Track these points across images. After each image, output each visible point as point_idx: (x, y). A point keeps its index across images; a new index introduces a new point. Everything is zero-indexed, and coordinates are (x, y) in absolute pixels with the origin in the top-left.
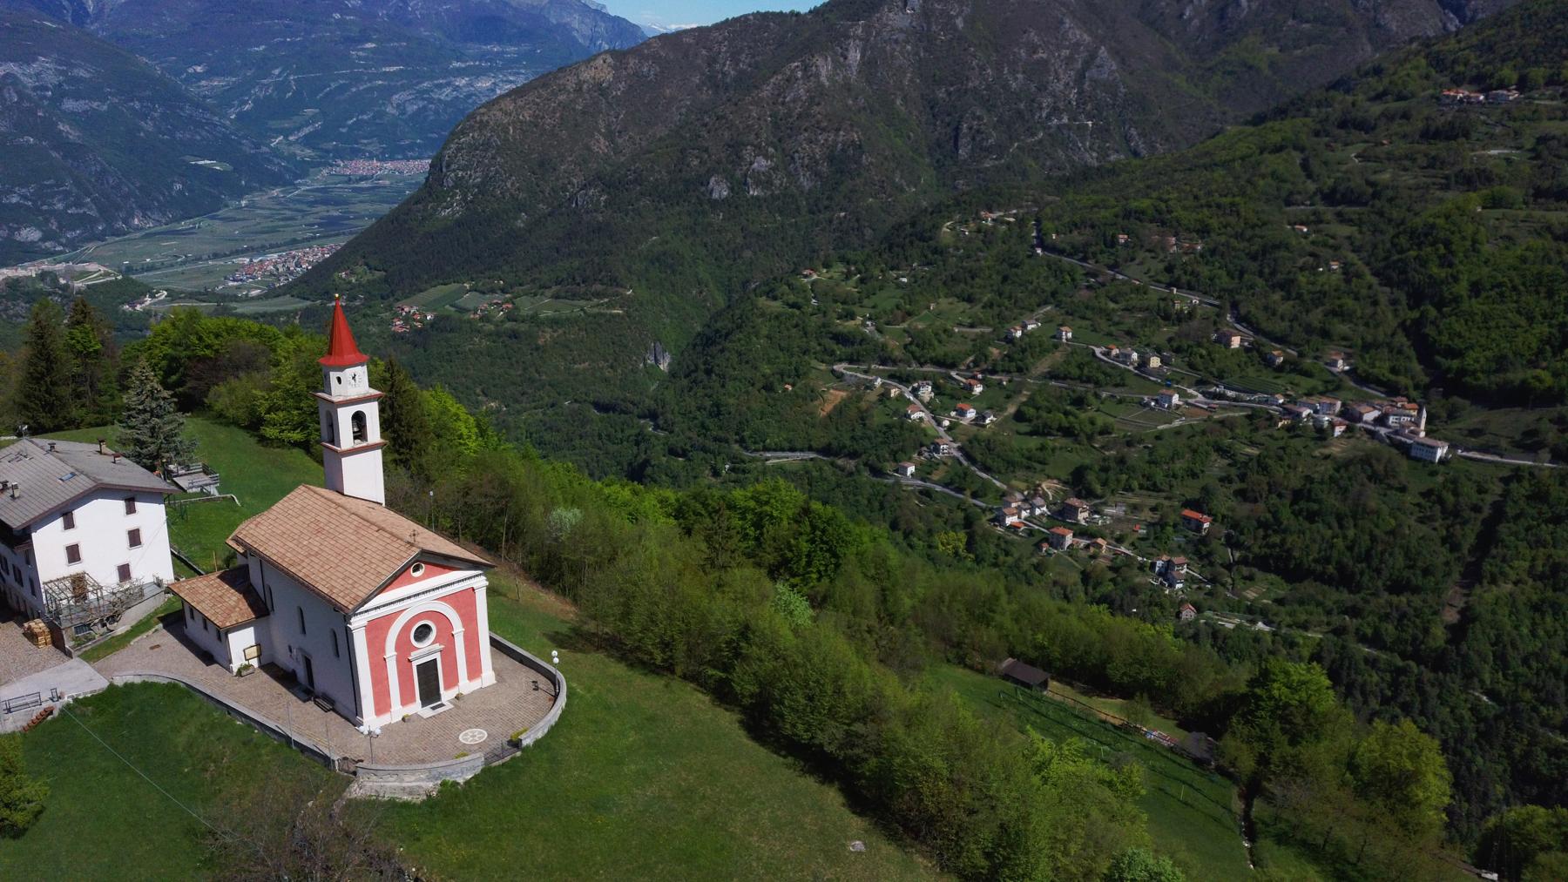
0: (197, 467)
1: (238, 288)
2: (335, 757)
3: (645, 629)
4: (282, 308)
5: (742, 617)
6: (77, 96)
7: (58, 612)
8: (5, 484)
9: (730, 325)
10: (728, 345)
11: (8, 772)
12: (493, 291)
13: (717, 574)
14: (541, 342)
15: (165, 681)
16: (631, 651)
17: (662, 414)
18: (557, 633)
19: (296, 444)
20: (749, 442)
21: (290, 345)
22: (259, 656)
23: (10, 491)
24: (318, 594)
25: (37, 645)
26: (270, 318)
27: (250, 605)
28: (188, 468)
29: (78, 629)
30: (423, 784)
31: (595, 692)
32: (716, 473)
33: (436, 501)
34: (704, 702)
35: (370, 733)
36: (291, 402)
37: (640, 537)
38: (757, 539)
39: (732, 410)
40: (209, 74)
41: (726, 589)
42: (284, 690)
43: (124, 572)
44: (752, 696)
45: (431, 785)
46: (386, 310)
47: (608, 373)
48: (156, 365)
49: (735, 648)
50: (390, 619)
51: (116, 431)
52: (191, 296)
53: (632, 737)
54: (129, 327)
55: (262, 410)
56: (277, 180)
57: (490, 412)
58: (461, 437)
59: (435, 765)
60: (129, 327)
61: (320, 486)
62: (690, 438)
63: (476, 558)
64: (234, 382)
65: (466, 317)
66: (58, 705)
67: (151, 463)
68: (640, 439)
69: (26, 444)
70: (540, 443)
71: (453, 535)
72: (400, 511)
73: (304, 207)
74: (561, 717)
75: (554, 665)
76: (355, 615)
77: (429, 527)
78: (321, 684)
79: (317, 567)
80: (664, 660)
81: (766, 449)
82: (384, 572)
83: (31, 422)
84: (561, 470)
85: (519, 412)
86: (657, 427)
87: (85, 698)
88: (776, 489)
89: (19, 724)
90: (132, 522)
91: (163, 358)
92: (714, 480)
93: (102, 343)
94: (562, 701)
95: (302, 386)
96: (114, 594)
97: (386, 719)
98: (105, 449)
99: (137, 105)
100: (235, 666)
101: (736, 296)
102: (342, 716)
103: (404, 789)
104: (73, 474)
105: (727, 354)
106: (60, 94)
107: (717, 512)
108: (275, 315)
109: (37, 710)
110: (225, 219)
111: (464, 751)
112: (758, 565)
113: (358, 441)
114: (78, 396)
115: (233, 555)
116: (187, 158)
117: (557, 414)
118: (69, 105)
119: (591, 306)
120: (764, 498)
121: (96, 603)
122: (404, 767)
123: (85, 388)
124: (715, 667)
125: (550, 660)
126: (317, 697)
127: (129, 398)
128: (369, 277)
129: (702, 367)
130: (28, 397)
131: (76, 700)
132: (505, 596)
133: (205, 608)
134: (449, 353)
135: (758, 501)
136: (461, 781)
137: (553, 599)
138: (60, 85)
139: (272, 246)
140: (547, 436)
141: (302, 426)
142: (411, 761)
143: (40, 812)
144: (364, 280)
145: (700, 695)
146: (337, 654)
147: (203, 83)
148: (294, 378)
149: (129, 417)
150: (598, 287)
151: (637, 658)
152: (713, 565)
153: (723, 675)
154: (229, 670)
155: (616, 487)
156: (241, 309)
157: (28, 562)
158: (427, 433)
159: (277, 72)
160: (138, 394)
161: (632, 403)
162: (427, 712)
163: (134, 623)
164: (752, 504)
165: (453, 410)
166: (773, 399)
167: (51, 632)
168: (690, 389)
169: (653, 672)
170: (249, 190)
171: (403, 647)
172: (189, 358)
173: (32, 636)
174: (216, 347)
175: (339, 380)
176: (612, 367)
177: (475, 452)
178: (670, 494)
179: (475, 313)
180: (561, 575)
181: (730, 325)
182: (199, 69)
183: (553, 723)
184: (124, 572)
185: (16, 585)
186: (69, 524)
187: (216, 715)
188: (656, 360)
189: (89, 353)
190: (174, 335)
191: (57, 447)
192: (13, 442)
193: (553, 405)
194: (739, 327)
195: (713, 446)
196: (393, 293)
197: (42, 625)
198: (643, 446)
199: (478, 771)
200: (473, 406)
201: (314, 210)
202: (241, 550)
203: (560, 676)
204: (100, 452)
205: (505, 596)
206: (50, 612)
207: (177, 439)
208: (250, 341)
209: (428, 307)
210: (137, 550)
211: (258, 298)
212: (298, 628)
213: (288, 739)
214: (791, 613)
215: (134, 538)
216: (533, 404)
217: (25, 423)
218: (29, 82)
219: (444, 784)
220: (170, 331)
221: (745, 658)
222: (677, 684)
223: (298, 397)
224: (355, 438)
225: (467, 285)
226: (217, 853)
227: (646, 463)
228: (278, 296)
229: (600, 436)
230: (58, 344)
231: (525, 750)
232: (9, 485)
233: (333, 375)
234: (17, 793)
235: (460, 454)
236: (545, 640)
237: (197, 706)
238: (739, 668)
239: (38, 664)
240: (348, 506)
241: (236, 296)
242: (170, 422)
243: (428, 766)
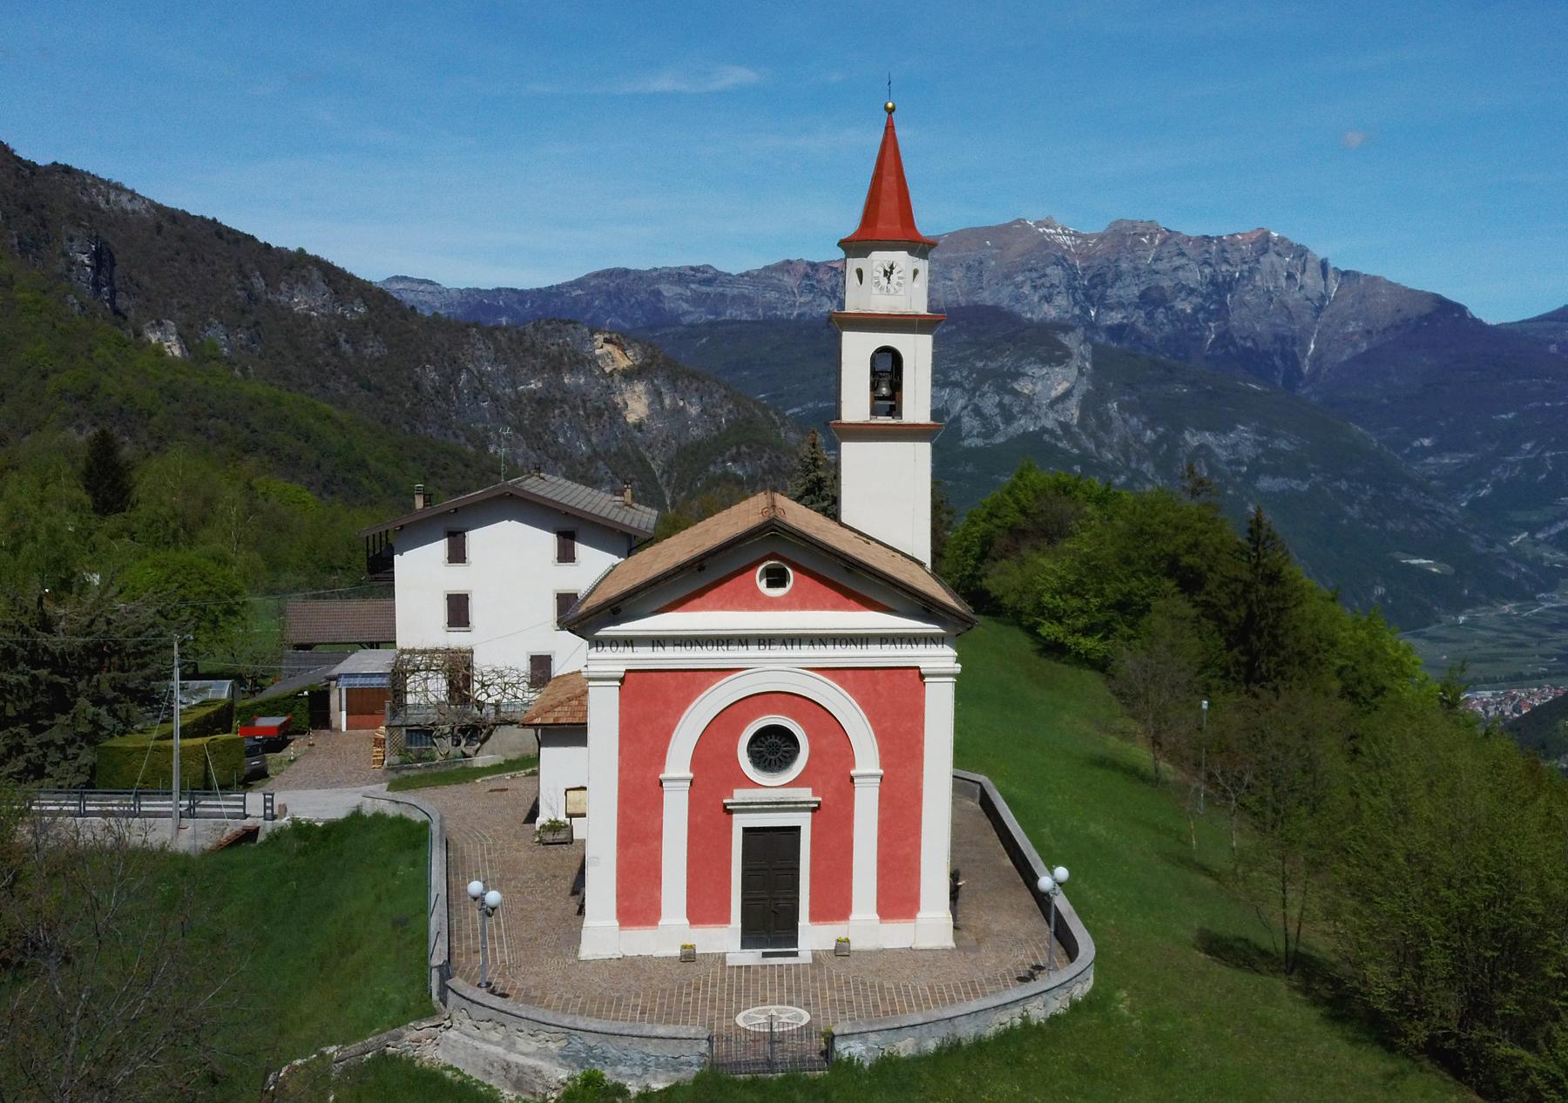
6: (1275, 472)
30: (544, 1065)
40: (1437, 450)
50: (697, 680)
56: (1510, 591)
73: (1544, 631)
89: (199, 843)
99: (1344, 485)
103: (507, 1067)
106: (1256, 470)
110: (1431, 639)
116: (1397, 555)
118: (1265, 483)
131: (296, 823)
136: (634, 1088)
138: (1258, 458)
139: (1487, 681)
147: (1431, 460)
159: (1528, 446)
170: (1472, 602)
175: (860, 273)
182: (1426, 442)
183: (967, 1032)
186: (457, 555)
199: (688, 1074)
201: (1557, 636)
218: (1223, 454)
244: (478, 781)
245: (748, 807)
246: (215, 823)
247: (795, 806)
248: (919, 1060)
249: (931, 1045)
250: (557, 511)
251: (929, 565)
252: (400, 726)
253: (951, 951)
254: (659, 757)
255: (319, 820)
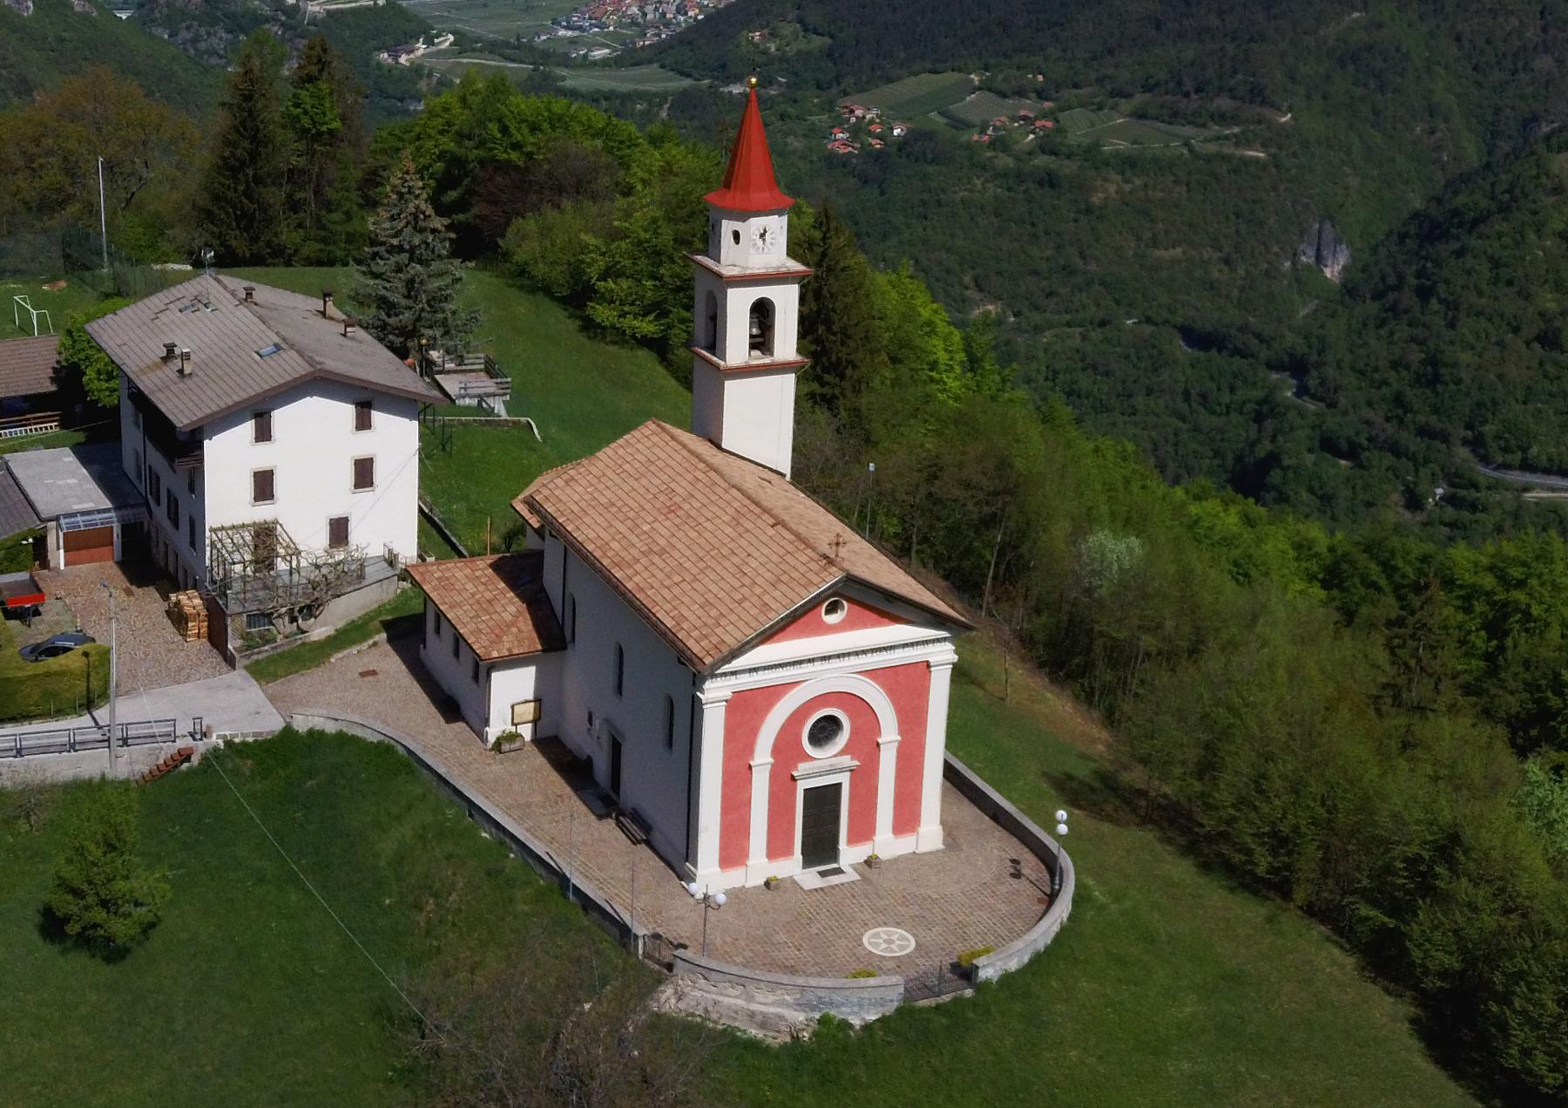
0: (476, 361)
1: (573, 42)
2: (640, 930)
3: (1241, 802)
4: (640, 87)
5: (1446, 816)
7: (225, 584)
8: (170, 349)
9: (1484, 203)
10: (1474, 242)
11: (111, 847)
12: (1021, 93)
13: (1402, 720)
14: (1097, 199)
15: (373, 738)
16: (1210, 839)
17: (1318, 366)
18: (1070, 777)
19: (645, 342)
20: (1493, 447)
21: (655, 158)
22: (535, 722)
23: (178, 362)
24: (655, 626)
25: (185, 636)
26: (618, 103)
27: (538, 626)
28: (460, 360)
29: (254, 619)
31: (1128, 904)
32: (1414, 502)
33: (877, 482)
34: (1342, 967)
35: (706, 897)
36: (643, 263)
37: (1255, 619)
38: (1489, 657)
39: (1465, 376)
41: (1418, 753)
42: (568, 790)
43: (339, 530)
44: (1444, 974)
45: (800, 1017)
46: (822, 110)
47: (1218, 273)
48: (426, 168)
49: (1423, 874)
50: (776, 692)
51: (350, 277)
52: (493, 48)
53: (1189, 1008)
54: (383, 93)
55: (593, 273)
57: (987, 323)
58: (933, 366)
59: (813, 982)
60: (383, 93)
61: (679, 425)
62: (1368, 423)
63: (942, 607)
64: (551, 215)
65: (964, 138)
66: (201, 747)
67: (401, 342)
68: (1265, 411)
69: (207, 283)
70: (1072, 394)
71: (900, 552)
72: (813, 492)
74: (1058, 938)
75: (1058, 837)
76: (713, 676)
77: (858, 528)
78: (633, 790)
79: (661, 576)
80: (1274, 870)
81: (1527, 466)
82: (774, 605)
83: (215, 242)
84: (1110, 455)
85: (1038, 329)
86: (1302, 391)
87: (244, 743)
88: (1544, 556)
90: (363, 445)
91: (441, 156)
92: (1408, 515)
93: (343, 118)
94: (1063, 909)
95: (667, 235)
96: (317, 567)
97: (736, 878)
98: (332, 310)
100: (493, 732)
101: (1505, 146)
102: (662, 858)
103: (752, 1015)
104: (278, 347)
105: (1470, 262)
107: (1418, 589)
108: (626, 98)
109: (169, 749)
111: (869, 967)
112: (1487, 713)
113: (756, 353)
114: (294, 206)
115: (521, 528)
117: (1107, 340)
119: (1203, 139)
120: (1516, 573)
121: (286, 578)
122: (758, 974)
123: (306, 194)
124: (1375, 904)
125: (1050, 827)
126: (621, 813)
127: (377, 223)
128: (802, 45)
129: (1413, 281)
130: (217, 198)
131: (229, 744)
132: (980, 686)
133: (461, 616)
134: (923, 203)
135: (1503, 579)
136: (856, 1022)
137: (1069, 707)
140: (1085, 382)
141: (657, 309)
142: (772, 965)
143: (152, 925)
144: (791, 50)
145: (1336, 952)
146: (670, 743)
148: (654, 221)
149: (375, 255)
150: (1224, 103)
151: (1220, 855)
152: (1397, 701)
153: (1391, 923)
154: (482, 737)
155: (1213, 505)
156: (573, 80)
157: (192, 489)
158: (874, 352)
160: (392, 218)
161: (1259, 336)
162: (810, 879)
163: (341, 624)
164: (1488, 581)
165: (926, 314)
166: (1556, 364)
167: (210, 617)
168: (1381, 324)
169: (1245, 887)
171: (786, 750)
172: (482, 162)
173: (178, 618)
174: (529, 148)
175: (736, 236)
176: (1227, 261)
177: (957, 398)
178: (1315, 531)
179: (983, 131)
180: (1088, 667)
181: (1484, 203)
183: (1041, 946)
184: (339, 530)
185: (166, 524)
186: (263, 434)
187: (450, 813)
188: (1319, 258)
189: (320, 134)
190: (461, 118)
191: (257, 296)
192: (182, 278)
193: (1103, 324)
194: (1504, 209)
195: (1415, 444)
196: (838, 79)
197: (197, 601)
198: (1269, 425)
199: (890, 1009)
200: (957, 305)
202: (535, 522)
203: (1065, 860)
204: (323, 314)
205: (980, 686)
206: (213, 582)
207: (450, 306)
208: (587, 143)
209: (896, 111)
210: (365, 496)
211: (604, 63)
212: (611, 681)
213: (564, 880)
214: (1550, 825)
215: (364, 473)
216: (1068, 317)
217: (211, 247)
219: (824, 1021)
220: (457, 110)
221: (1443, 899)
222: (1291, 920)
223: (657, 255)
224: (753, 346)
225: (975, 78)
226: (423, 1062)
227: (1273, 459)
228: (637, 64)
229: (1187, 396)
230: (274, 112)
231: (984, 987)
232: (177, 351)
233: (727, 227)
234: (121, 885)
235: (928, 398)
236: (1045, 786)
237: (420, 791)
238: (1425, 915)
239: (181, 669)
240: (726, 470)
241: (566, 55)
242: (440, 275)
243: (801, 981)
244: (332, 660)
245: (808, 776)
246: (150, 749)
247: (842, 770)
248: (1022, 971)
249: (1026, 960)
250: (352, 386)
251: (788, 477)
252: (241, 613)
253: (943, 851)
254: (749, 749)
255: (247, 735)
